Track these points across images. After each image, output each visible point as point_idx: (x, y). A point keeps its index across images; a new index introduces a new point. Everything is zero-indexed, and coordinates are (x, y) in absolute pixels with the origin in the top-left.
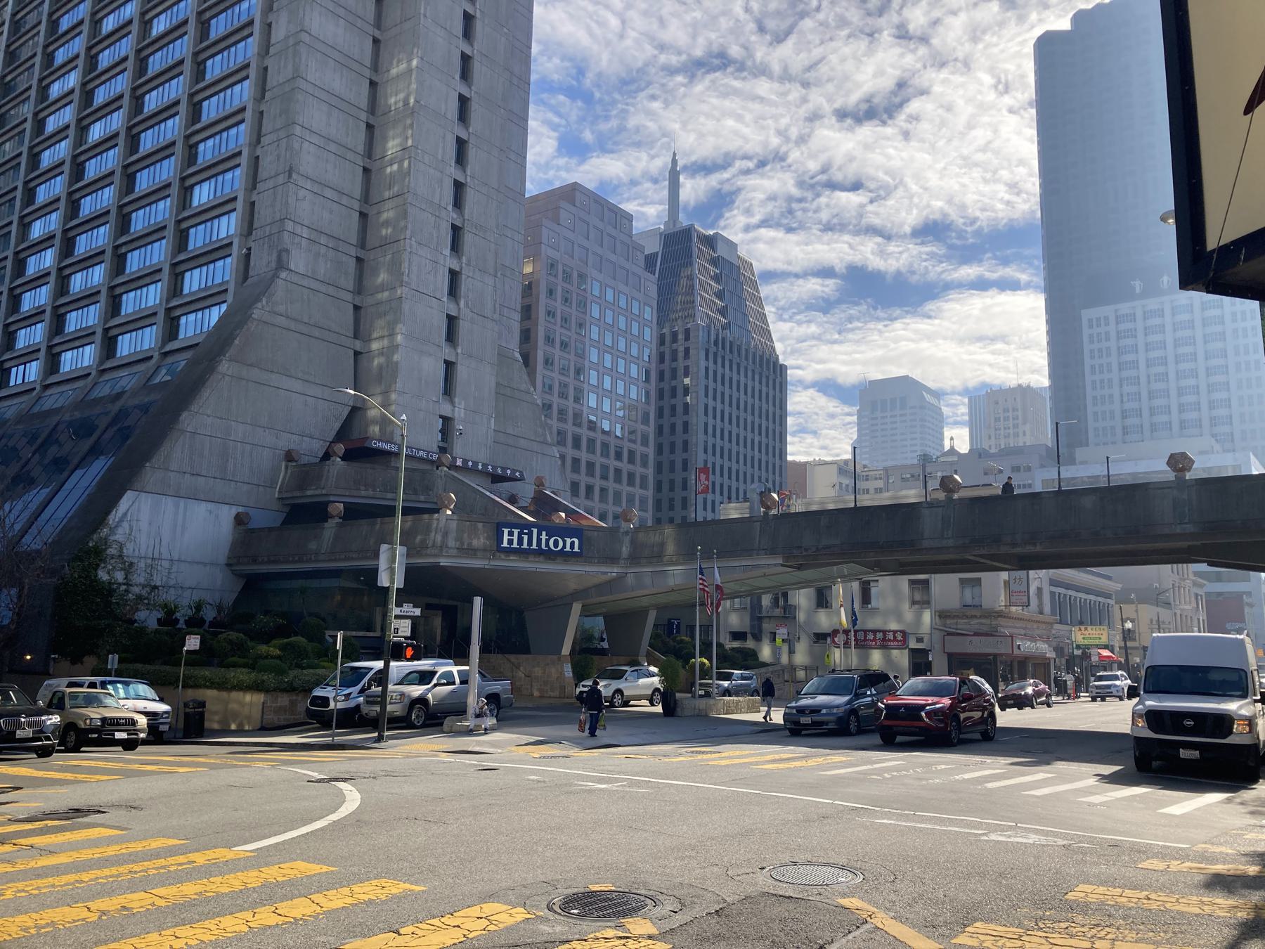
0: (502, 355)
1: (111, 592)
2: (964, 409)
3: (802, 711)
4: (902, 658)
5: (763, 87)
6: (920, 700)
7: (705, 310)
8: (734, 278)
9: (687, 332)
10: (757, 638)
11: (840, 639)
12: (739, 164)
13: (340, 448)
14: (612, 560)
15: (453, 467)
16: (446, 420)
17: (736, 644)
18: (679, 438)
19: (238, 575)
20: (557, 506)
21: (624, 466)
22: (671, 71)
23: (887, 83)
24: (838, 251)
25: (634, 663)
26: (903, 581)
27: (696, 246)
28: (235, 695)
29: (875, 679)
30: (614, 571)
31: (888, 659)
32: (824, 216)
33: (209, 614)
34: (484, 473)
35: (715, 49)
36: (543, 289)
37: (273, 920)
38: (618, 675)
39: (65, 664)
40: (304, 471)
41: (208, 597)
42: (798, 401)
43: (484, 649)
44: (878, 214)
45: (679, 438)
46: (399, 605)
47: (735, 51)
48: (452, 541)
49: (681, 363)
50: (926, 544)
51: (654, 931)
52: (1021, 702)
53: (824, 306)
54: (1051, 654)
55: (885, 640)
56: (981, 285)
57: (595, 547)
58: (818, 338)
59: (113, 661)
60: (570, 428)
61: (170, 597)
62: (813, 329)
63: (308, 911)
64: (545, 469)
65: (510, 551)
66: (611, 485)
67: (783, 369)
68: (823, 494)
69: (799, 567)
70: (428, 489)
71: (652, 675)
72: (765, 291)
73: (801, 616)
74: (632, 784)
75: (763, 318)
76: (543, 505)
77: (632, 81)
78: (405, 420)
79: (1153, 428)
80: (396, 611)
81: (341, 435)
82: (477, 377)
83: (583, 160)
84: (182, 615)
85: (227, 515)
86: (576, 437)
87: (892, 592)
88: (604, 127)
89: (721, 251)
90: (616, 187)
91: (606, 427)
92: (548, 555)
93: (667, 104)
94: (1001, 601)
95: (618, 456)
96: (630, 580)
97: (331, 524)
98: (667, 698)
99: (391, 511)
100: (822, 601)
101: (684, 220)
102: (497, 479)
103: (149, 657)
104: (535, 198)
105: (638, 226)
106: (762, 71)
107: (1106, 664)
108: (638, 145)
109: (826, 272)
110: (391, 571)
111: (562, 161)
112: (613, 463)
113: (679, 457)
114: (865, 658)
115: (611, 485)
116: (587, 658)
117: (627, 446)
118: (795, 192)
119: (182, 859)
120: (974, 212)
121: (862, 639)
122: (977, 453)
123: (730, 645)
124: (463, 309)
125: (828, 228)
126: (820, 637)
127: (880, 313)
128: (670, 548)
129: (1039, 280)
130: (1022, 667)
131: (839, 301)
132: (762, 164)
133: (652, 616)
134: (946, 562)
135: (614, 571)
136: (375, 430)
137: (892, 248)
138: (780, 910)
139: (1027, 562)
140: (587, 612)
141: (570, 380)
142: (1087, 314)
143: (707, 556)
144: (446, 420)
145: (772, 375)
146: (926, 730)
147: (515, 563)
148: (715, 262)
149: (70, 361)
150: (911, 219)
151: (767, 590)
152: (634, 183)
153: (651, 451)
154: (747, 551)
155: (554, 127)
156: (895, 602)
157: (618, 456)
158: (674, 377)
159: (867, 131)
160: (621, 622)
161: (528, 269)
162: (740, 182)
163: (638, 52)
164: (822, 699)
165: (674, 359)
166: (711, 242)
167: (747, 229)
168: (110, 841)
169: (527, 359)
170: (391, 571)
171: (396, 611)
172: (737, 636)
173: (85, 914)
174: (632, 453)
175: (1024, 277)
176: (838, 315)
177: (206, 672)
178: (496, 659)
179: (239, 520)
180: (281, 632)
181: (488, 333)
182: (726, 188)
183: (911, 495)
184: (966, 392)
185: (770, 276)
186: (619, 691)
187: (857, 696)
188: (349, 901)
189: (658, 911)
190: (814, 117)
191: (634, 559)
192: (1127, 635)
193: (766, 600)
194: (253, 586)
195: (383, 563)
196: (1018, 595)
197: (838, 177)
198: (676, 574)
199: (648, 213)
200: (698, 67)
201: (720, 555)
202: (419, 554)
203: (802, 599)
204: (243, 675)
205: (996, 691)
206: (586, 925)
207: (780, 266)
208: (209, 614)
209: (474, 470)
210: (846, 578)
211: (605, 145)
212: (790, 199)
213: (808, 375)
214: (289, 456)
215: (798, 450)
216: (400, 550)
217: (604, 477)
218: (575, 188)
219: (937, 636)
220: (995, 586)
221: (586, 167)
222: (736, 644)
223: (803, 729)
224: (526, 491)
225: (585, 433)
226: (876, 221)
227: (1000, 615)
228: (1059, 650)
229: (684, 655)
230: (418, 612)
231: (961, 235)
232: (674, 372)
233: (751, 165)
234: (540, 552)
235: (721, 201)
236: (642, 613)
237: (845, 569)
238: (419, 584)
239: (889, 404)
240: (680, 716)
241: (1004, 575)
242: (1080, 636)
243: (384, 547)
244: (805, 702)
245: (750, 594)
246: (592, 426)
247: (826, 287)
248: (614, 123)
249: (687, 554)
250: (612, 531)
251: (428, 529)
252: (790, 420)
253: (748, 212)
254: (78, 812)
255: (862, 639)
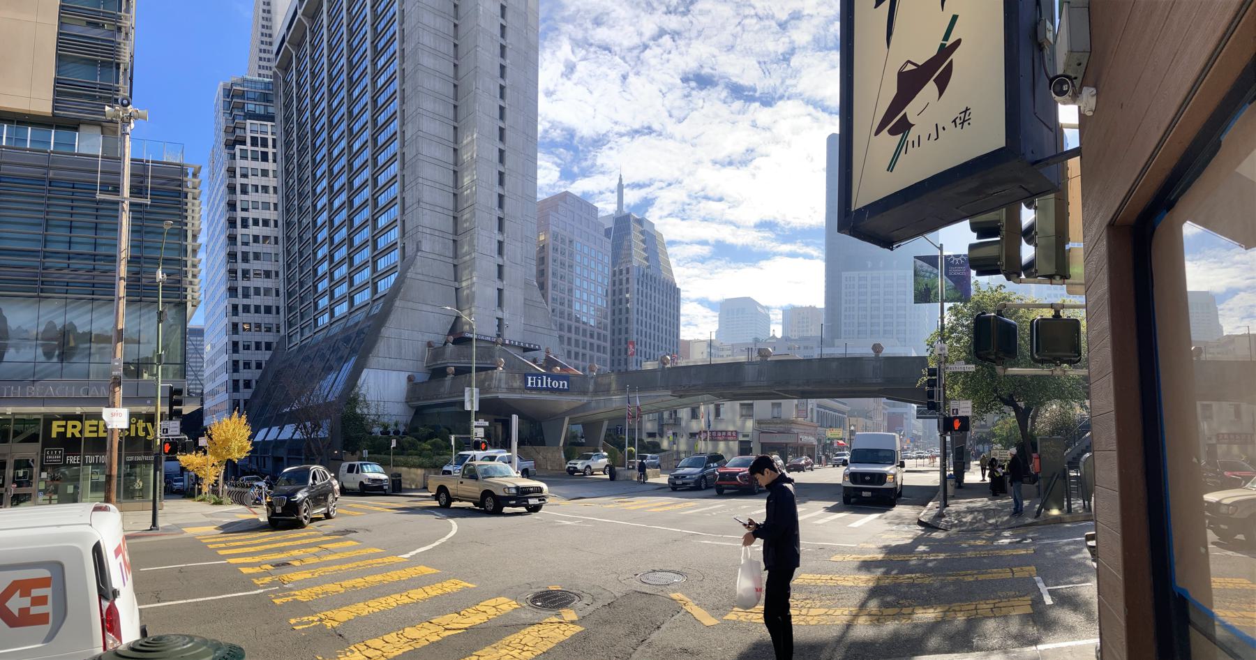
0: (527, 284)
1: (363, 419)
2: (780, 317)
3: (677, 477)
4: (735, 446)
5: (670, 144)
6: (736, 470)
7: (638, 258)
8: (652, 241)
9: (628, 270)
10: (661, 436)
11: (702, 436)
12: (657, 184)
13: (451, 338)
14: (584, 393)
15: (503, 344)
16: (500, 320)
17: (650, 440)
18: (623, 326)
19: (412, 407)
20: (556, 363)
21: (595, 341)
22: (621, 135)
23: (741, 149)
24: (712, 232)
25: (596, 451)
26: (737, 404)
27: (633, 225)
28: (413, 470)
29: (716, 458)
30: (585, 399)
31: (728, 447)
32: (702, 213)
33: (402, 429)
34: (519, 347)
35: (646, 124)
36: (551, 247)
37: (407, 600)
38: (588, 458)
39: (349, 455)
40: (435, 351)
41: (398, 418)
42: (686, 309)
43: (521, 443)
44: (732, 215)
45: (623, 326)
46: (476, 420)
47: (656, 126)
48: (503, 385)
49: (624, 286)
50: (746, 384)
51: (575, 618)
52: (799, 468)
53: (702, 260)
54: (815, 443)
55: (726, 436)
56: (793, 255)
57: (575, 385)
58: (698, 276)
59: (365, 452)
60: (566, 322)
61: (385, 420)
62: (696, 271)
63: (420, 597)
64: (550, 344)
65: (532, 389)
66: (588, 352)
67: (678, 290)
68: (698, 357)
69: (681, 397)
70: (492, 357)
71: (604, 457)
72: (670, 250)
73: (683, 424)
74: (586, 521)
75: (669, 264)
76: (550, 363)
77: (599, 140)
78: (479, 322)
79: (885, 332)
80: (475, 423)
81: (452, 331)
82: (514, 296)
83: (573, 182)
84: (391, 429)
85: (404, 376)
86: (568, 327)
87: (731, 409)
88: (584, 164)
89: (646, 227)
90: (591, 195)
91: (585, 319)
92: (552, 390)
93: (619, 152)
94: (793, 415)
95: (592, 336)
96: (593, 404)
97: (449, 377)
98: (611, 469)
99: (469, 370)
100: (694, 415)
101: (626, 210)
102: (526, 350)
103: (379, 452)
104: (545, 201)
105: (600, 214)
106: (671, 137)
107: (842, 448)
108: (603, 173)
109: (703, 243)
110: (471, 401)
111: (562, 183)
112: (589, 340)
113: (623, 336)
114: (716, 447)
115: (588, 352)
116: (574, 448)
117: (596, 330)
118: (688, 201)
119: (380, 560)
120: (789, 219)
121: (715, 436)
122: (785, 338)
123: (647, 440)
124: (506, 261)
125: (704, 220)
126: (693, 435)
127: (733, 265)
128: (614, 386)
129: (823, 256)
130: (799, 450)
131: (711, 258)
132: (670, 185)
133: (606, 424)
134: (763, 394)
135: (585, 399)
136: (467, 328)
137: (740, 232)
138: (640, 602)
139: (805, 395)
140: (572, 422)
141: (566, 296)
142: (845, 274)
143: (632, 390)
144: (500, 320)
145: (672, 294)
146: (738, 486)
147: (534, 396)
148: (642, 233)
149: (359, 299)
150: (755, 219)
151: (667, 409)
152: (601, 193)
153: (608, 333)
154: (654, 388)
155: (558, 165)
156: (732, 416)
157: (592, 336)
158: (621, 293)
159: (729, 171)
160: (591, 427)
161: (542, 238)
162: (658, 193)
163: (602, 126)
164: (687, 470)
165: (621, 284)
166: (640, 222)
167: (661, 218)
168: (354, 548)
169: (542, 286)
170: (471, 401)
171: (475, 423)
172: (651, 435)
173: (339, 588)
174: (599, 334)
175: (815, 254)
176: (709, 265)
177: (401, 458)
178: (528, 448)
179: (410, 379)
180: (431, 436)
181: (520, 272)
182: (650, 196)
183: (742, 358)
184: (781, 308)
185: (672, 243)
186: (589, 466)
187: (706, 468)
188: (440, 592)
189: (580, 605)
190: (699, 162)
191: (596, 392)
192: (852, 433)
193: (666, 415)
194: (419, 412)
195: (467, 398)
196: (801, 412)
197: (711, 194)
198: (617, 400)
199: (607, 207)
200: (635, 133)
201: (640, 390)
202: (487, 392)
203: (684, 414)
204: (416, 460)
205: (785, 462)
206: (543, 613)
207: (678, 238)
208: (402, 429)
209: (514, 346)
210: (705, 403)
211: (585, 173)
212: (684, 204)
213: (694, 294)
214: (429, 344)
215: (686, 334)
216: (475, 390)
217: (584, 348)
218: (567, 194)
219: (756, 433)
220: (790, 408)
221: (574, 185)
222: (650, 440)
223: (678, 487)
224: (541, 356)
225: (574, 324)
226: (732, 218)
227: (793, 422)
228: (819, 441)
229: (621, 447)
230: (487, 424)
231: (782, 229)
232: (621, 291)
233: (664, 185)
234: (547, 389)
235: (647, 203)
236: (600, 422)
237: (706, 397)
238: (489, 408)
239: (736, 311)
240: (625, 480)
241: (796, 401)
242: (830, 433)
243: (467, 389)
244: (680, 471)
245: (656, 411)
246: (578, 320)
247: (705, 250)
248: (589, 163)
249: (622, 390)
250: (585, 376)
251: (491, 379)
252: (682, 319)
253: (661, 208)
254: (347, 532)
255: (715, 436)
